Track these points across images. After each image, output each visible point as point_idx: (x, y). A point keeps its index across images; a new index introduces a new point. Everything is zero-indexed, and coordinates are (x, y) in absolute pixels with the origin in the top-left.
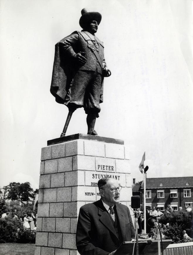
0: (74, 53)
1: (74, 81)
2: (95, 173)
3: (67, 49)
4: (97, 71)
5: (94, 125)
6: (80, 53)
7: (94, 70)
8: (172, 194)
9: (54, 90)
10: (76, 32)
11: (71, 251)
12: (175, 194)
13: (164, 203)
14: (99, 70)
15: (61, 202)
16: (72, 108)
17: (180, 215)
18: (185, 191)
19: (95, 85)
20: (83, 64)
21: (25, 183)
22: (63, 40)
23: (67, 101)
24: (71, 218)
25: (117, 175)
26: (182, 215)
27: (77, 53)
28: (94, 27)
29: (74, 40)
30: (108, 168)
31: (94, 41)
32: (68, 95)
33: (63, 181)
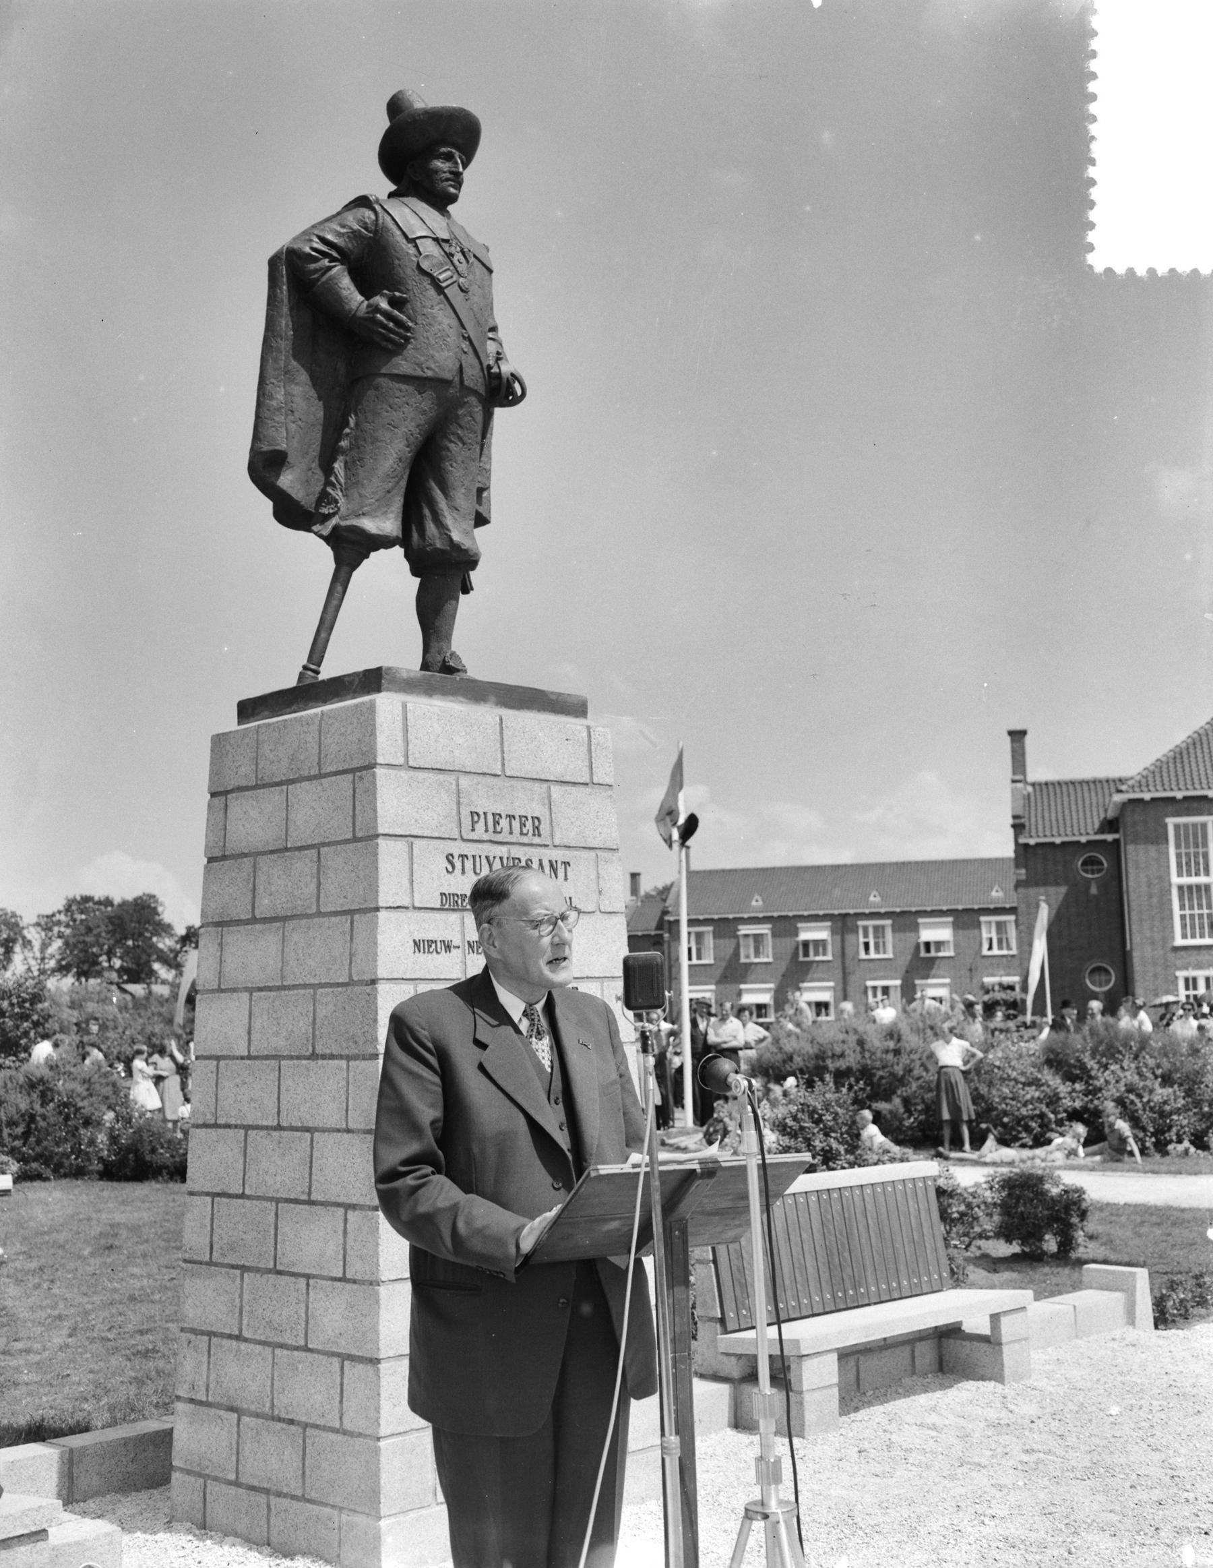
1: (357, 424)
2: (457, 848)
6: (383, 295)
7: (448, 376)
8: (806, 944)
9: (265, 467)
10: (363, 202)
11: (350, 1214)
12: (939, 945)
14: (473, 377)
16: (351, 548)
17: (843, 1042)
18: (865, 929)
19: (452, 446)
21: (136, 900)
22: (306, 235)
23: (326, 518)
24: (348, 1058)
25: (558, 855)
26: (852, 1039)
27: (368, 298)
28: (448, 175)
29: (355, 235)
30: (516, 824)
31: (447, 241)
32: (329, 490)
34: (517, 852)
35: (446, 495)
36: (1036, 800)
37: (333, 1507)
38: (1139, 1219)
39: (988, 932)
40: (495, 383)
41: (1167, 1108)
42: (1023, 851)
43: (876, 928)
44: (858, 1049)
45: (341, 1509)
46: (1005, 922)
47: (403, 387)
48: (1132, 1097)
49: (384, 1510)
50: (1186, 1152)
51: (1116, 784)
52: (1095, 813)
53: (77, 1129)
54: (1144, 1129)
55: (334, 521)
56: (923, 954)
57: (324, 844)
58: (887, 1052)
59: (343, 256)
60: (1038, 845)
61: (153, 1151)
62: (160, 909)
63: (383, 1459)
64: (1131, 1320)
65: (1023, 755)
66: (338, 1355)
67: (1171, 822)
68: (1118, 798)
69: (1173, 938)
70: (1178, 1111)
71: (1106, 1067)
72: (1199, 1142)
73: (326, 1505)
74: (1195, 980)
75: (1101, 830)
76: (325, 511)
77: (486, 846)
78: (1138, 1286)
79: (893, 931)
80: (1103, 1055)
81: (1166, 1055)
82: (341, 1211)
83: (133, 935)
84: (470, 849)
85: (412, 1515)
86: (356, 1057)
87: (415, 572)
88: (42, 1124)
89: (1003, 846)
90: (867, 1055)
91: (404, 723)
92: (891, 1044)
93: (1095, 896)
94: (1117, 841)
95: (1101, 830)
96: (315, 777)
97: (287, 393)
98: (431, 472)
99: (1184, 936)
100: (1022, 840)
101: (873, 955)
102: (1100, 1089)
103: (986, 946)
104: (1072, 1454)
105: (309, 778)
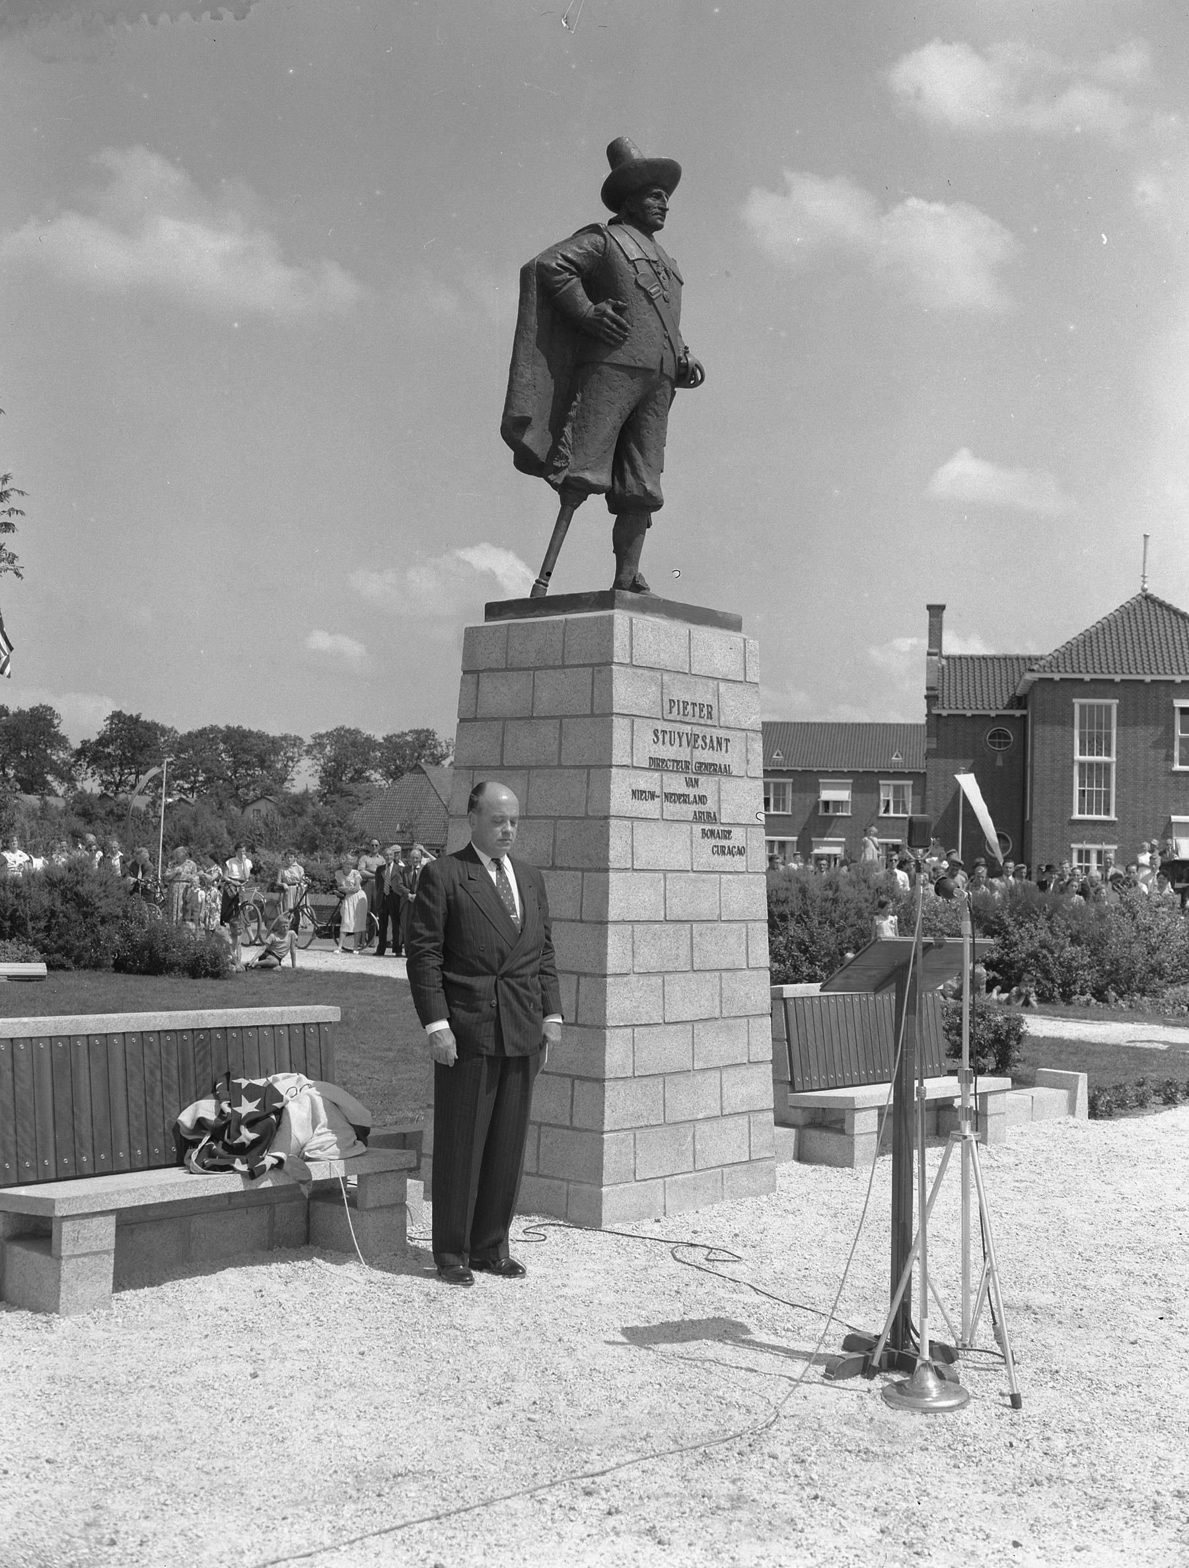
0: (587, 306)
1: (582, 400)
2: (660, 725)
3: (565, 288)
4: (662, 370)
5: (639, 554)
6: (608, 302)
7: (653, 367)
9: (513, 429)
10: (594, 229)
11: (582, 980)
12: (838, 804)
13: (795, 838)
14: (670, 369)
15: (547, 817)
16: (572, 494)
17: (787, 889)
19: (649, 417)
20: (618, 344)
21: (32, 710)
22: (551, 252)
23: (557, 470)
24: (583, 870)
25: (722, 733)
26: (795, 887)
27: (595, 304)
28: (657, 210)
29: (589, 255)
30: (697, 709)
31: (655, 262)
32: (560, 448)
33: (555, 747)
34: (698, 730)
35: (642, 453)
36: (948, 674)
37: (562, 1180)
38: (1057, 1050)
39: (886, 794)
40: (683, 370)
41: (1075, 964)
42: (934, 720)
43: (777, 785)
44: (800, 896)
45: (569, 1181)
46: (903, 786)
47: (620, 373)
48: (1045, 952)
49: (605, 1181)
50: (1088, 1003)
51: (1029, 662)
52: (1004, 689)
53: (95, 926)
54: (1053, 981)
55: (565, 473)
56: (821, 813)
57: (566, 717)
58: (826, 900)
59: (579, 270)
60: (949, 715)
61: (166, 949)
62: (56, 721)
63: (605, 1147)
64: (1072, 1110)
65: (940, 629)
66: (569, 1076)
67: (1077, 702)
68: (1029, 676)
69: (1071, 813)
70: (1083, 967)
71: (1021, 925)
72: (1099, 994)
73: (557, 1179)
74: (1088, 852)
75: (1010, 706)
76: (557, 464)
77: (678, 725)
78: (1080, 1086)
79: (794, 791)
80: (1020, 914)
81: (1075, 918)
82: (575, 977)
83: (27, 745)
84: (668, 727)
85: (621, 1186)
86: (589, 870)
87: (612, 510)
88: (62, 920)
89: (917, 713)
90: (808, 902)
91: (635, 634)
92: (830, 894)
93: (1000, 768)
94: (1024, 717)
95: (1010, 706)
96: (559, 667)
97: (534, 374)
98: (635, 439)
99: (1081, 812)
100: (934, 712)
101: (892, 814)
102: (1016, 944)
103: (883, 809)
104: (1049, 1184)
105: (553, 668)
